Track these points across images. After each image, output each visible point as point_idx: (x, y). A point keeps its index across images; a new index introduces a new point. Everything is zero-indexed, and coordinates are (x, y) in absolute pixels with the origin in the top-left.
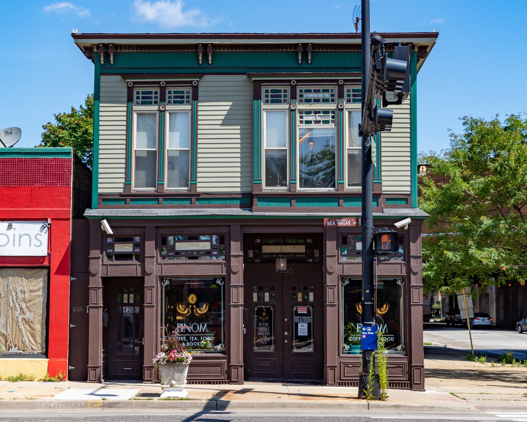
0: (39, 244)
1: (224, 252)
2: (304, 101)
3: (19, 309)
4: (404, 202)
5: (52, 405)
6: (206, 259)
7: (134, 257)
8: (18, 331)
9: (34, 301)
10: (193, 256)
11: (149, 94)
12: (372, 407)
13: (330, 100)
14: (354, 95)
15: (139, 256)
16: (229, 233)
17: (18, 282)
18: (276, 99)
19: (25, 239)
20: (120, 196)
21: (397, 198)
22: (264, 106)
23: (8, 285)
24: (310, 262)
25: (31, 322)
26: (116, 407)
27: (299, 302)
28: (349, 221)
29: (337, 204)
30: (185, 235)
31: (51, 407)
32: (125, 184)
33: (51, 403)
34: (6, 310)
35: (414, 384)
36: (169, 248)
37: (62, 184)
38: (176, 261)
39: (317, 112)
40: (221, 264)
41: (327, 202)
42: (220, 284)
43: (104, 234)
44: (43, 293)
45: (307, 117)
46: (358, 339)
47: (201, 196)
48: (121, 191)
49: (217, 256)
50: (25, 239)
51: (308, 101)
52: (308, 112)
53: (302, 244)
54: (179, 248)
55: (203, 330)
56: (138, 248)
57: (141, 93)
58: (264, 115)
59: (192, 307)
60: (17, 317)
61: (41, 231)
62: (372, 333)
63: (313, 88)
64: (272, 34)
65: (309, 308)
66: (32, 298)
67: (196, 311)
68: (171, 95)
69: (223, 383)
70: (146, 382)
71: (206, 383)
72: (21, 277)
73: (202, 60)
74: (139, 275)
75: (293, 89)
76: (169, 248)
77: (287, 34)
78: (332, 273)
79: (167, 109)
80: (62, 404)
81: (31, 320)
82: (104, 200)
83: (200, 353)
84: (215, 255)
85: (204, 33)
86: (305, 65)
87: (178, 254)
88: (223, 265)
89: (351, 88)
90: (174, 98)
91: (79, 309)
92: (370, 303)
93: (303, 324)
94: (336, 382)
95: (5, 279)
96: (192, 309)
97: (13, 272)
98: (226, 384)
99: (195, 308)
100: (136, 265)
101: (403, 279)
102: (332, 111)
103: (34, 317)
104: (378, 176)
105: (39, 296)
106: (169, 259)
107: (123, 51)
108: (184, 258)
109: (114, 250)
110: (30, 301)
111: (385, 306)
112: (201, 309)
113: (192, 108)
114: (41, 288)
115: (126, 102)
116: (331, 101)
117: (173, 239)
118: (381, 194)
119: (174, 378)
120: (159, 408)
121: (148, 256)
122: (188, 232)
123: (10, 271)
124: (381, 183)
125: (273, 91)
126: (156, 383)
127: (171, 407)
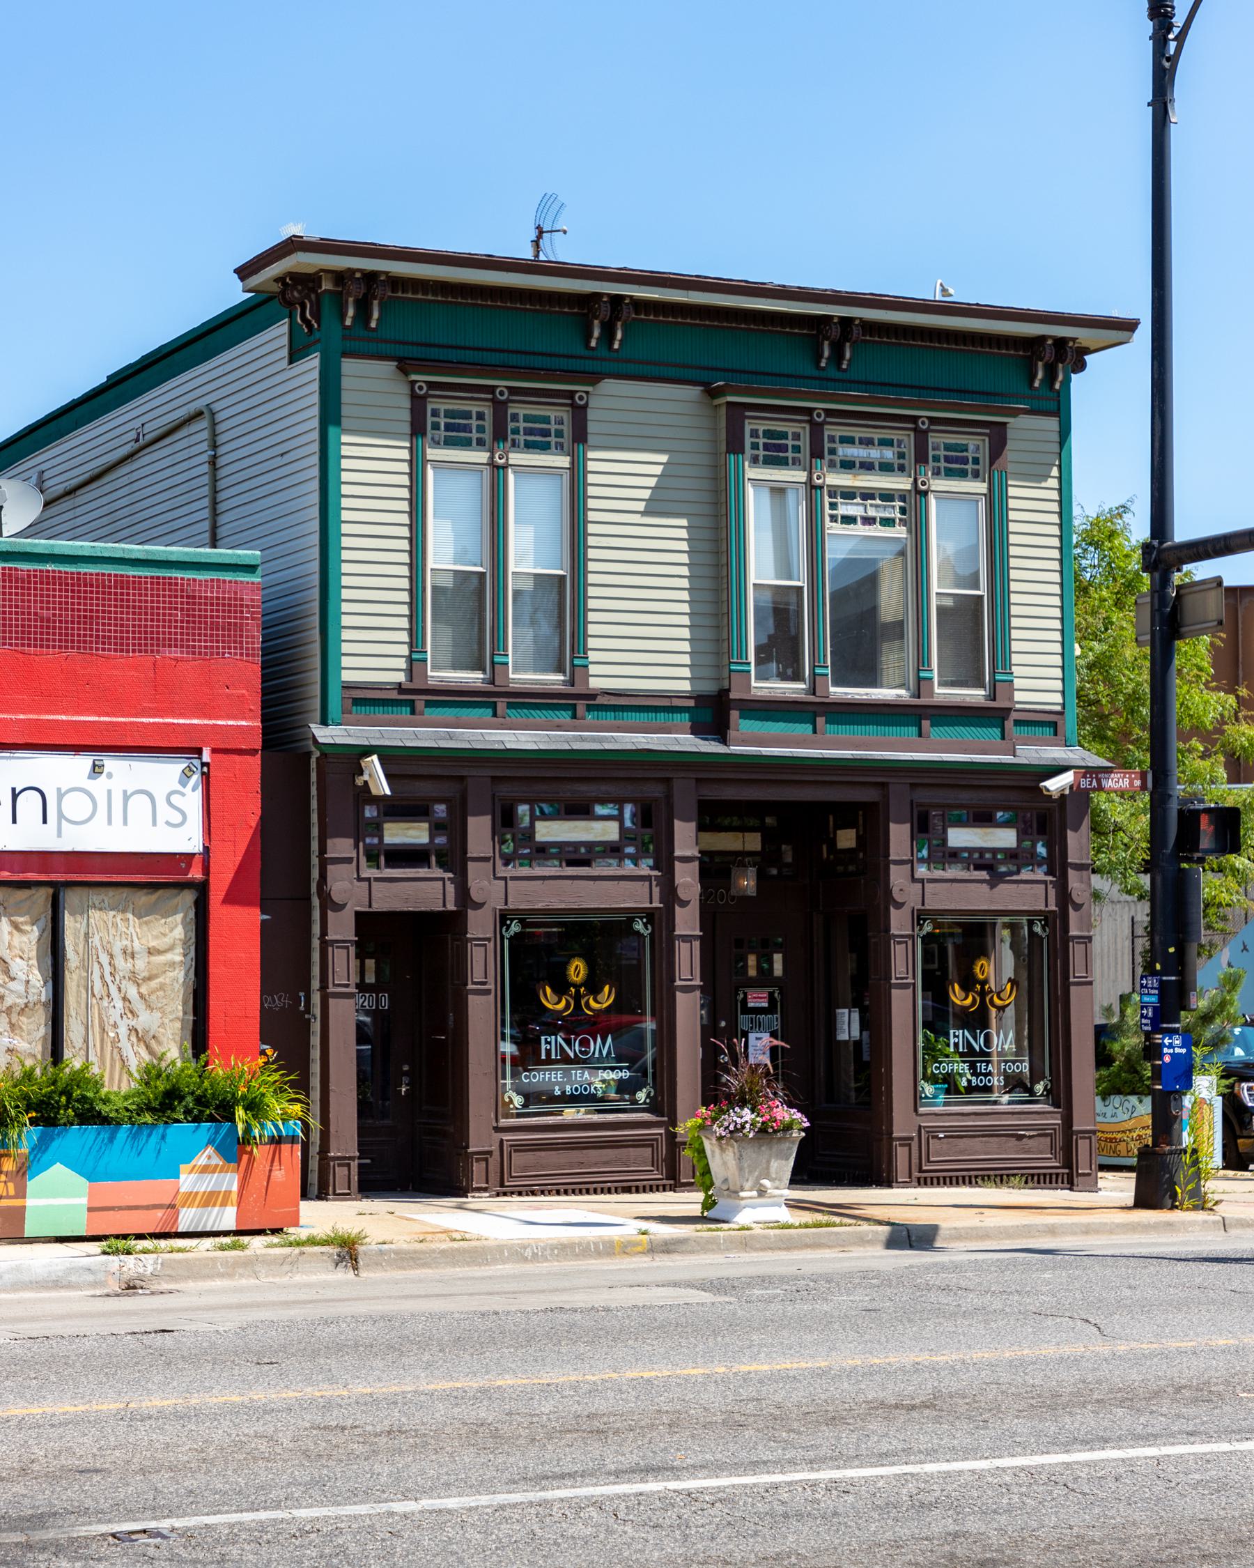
0: (177, 818)
1: (651, 847)
2: (838, 465)
3: (119, 1004)
4: (1048, 731)
5: (528, 1253)
6: (610, 865)
7: (433, 859)
8: (118, 1065)
9: (161, 980)
10: (577, 855)
11: (463, 418)
12: (1231, 1226)
13: (896, 466)
14: (947, 459)
15: (446, 855)
16: (669, 797)
17: (115, 925)
18: (775, 456)
19: (139, 805)
20: (399, 693)
21: (1028, 721)
22: (751, 472)
23: (87, 935)
24: (773, 876)
25: (154, 1037)
26: (682, 1252)
27: (751, 978)
28: (1124, 777)
29: (996, 732)
30: (558, 801)
31: (526, 1260)
32: (410, 660)
33: (525, 1248)
34: (83, 1006)
35: (1079, 1175)
36: (520, 836)
37: (236, 654)
38: (538, 871)
39: (867, 495)
40: (648, 878)
41: (834, 724)
42: (642, 931)
43: (364, 793)
44: (185, 955)
45: (844, 507)
46: (544, 1078)
47: (599, 700)
48: (400, 677)
49: (635, 860)
50: (139, 805)
51: (848, 465)
52: (849, 494)
53: (752, 829)
54: (543, 836)
55: (605, 1053)
56: (443, 835)
57: (442, 414)
58: (750, 491)
59: (578, 992)
60: (115, 1026)
61: (184, 785)
62: (1184, 1051)
63: (857, 433)
64: (784, 286)
65: (774, 992)
66: (155, 972)
67: (587, 1004)
68: (517, 424)
69: (658, 1190)
70: (477, 1195)
71: (619, 1190)
72: (124, 911)
73: (354, 318)
74: (451, 907)
75: (817, 430)
76: (520, 836)
77: (818, 289)
78: (903, 904)
79: (511, 462)
80: (552, 1250)
81: (151, 1034)
82: (357, 702)
83: (587, 1113)
84: (630, 856)
85: (625, 269)
86: (833, 373)
87: (543, 851)
88: (654, 883)
89: (942, 440)
90: (525, 434)
91: (279, 1000)
92: (1173, 978)
93: (759, 1035)
94: (913, 1177)
95: (79, 918)
96: (578, 998)
97: (100, 897)
98: (664, 1190)
99: (584, 996)
100: (443, 879)
101: (1046, 919)
102: (900, 496)
103: (162, 1025)
104: (1004, 667)
105: (172, 965)
106: (521, 865)
107: (547, 308)
108: (557, 863)
109: (381, 838)
110: (150, 978)
111: (607, 988)
112: (599, 998)
113: (572, 463)
114: (178, 942)
115: (409, 437)
116: (899, 470)
117: (528, 813)
118: (1010, 709)
119: (768, 1172)
120: (780, 1249)
121: (897, 858)
122: (568, 794)
123: (95, 896)
124: (1012, 681)
125: (768, 434)
126: (498, 1195)
127: (807, 1246)
